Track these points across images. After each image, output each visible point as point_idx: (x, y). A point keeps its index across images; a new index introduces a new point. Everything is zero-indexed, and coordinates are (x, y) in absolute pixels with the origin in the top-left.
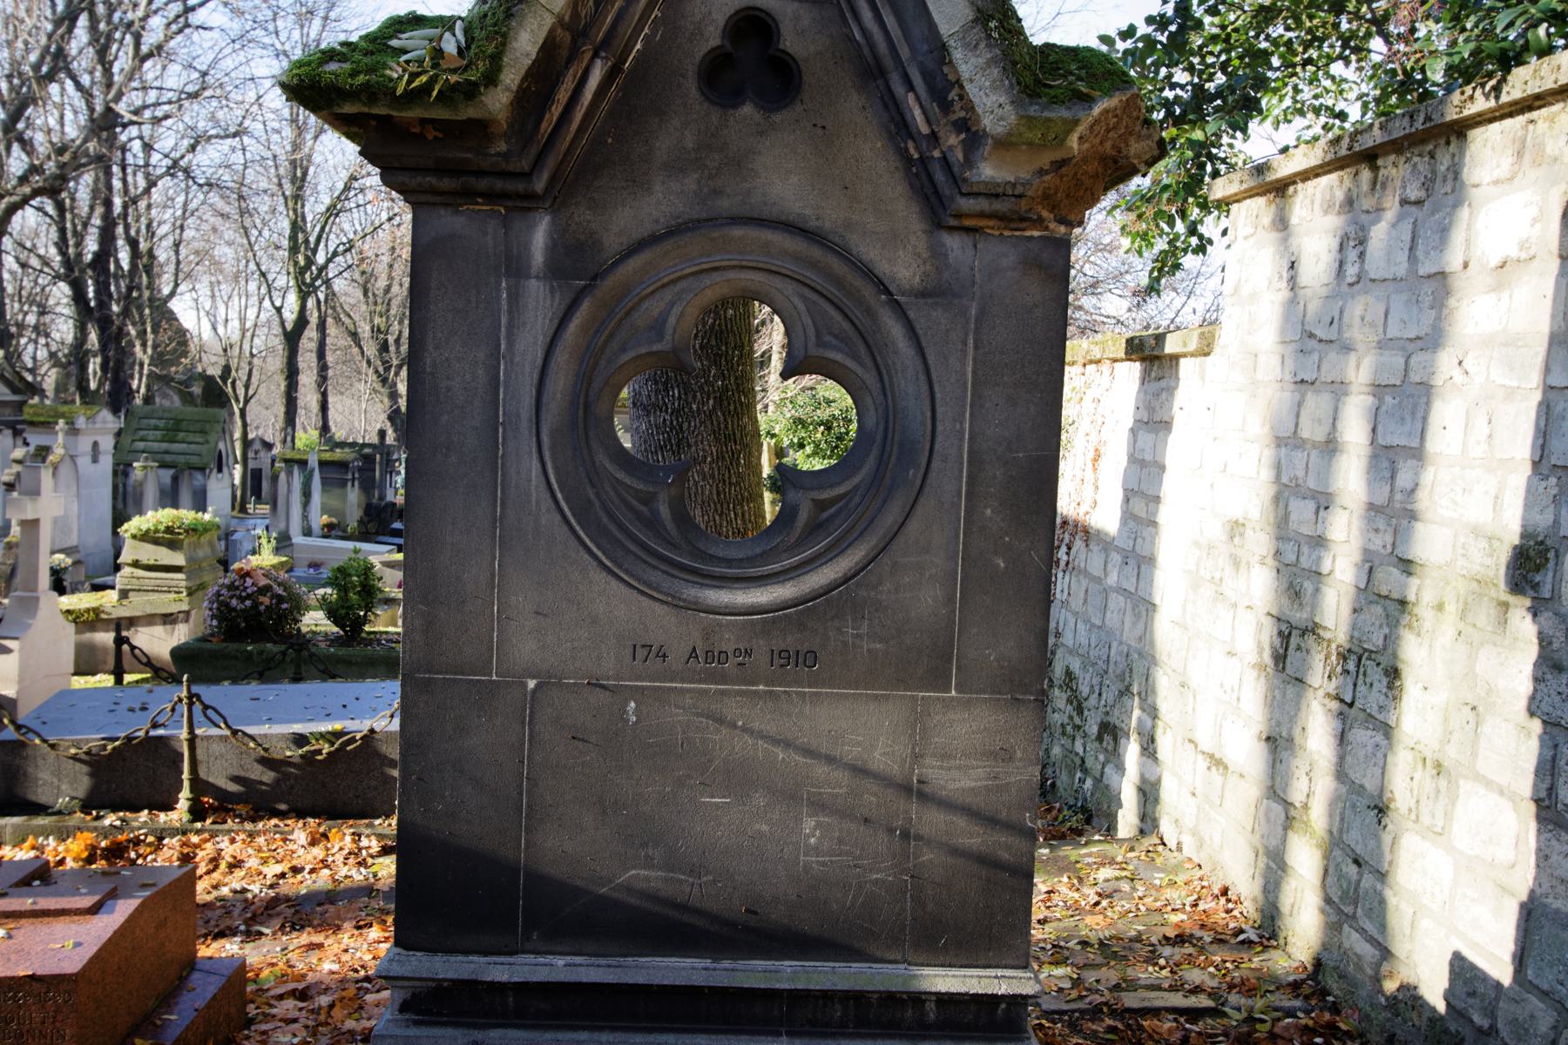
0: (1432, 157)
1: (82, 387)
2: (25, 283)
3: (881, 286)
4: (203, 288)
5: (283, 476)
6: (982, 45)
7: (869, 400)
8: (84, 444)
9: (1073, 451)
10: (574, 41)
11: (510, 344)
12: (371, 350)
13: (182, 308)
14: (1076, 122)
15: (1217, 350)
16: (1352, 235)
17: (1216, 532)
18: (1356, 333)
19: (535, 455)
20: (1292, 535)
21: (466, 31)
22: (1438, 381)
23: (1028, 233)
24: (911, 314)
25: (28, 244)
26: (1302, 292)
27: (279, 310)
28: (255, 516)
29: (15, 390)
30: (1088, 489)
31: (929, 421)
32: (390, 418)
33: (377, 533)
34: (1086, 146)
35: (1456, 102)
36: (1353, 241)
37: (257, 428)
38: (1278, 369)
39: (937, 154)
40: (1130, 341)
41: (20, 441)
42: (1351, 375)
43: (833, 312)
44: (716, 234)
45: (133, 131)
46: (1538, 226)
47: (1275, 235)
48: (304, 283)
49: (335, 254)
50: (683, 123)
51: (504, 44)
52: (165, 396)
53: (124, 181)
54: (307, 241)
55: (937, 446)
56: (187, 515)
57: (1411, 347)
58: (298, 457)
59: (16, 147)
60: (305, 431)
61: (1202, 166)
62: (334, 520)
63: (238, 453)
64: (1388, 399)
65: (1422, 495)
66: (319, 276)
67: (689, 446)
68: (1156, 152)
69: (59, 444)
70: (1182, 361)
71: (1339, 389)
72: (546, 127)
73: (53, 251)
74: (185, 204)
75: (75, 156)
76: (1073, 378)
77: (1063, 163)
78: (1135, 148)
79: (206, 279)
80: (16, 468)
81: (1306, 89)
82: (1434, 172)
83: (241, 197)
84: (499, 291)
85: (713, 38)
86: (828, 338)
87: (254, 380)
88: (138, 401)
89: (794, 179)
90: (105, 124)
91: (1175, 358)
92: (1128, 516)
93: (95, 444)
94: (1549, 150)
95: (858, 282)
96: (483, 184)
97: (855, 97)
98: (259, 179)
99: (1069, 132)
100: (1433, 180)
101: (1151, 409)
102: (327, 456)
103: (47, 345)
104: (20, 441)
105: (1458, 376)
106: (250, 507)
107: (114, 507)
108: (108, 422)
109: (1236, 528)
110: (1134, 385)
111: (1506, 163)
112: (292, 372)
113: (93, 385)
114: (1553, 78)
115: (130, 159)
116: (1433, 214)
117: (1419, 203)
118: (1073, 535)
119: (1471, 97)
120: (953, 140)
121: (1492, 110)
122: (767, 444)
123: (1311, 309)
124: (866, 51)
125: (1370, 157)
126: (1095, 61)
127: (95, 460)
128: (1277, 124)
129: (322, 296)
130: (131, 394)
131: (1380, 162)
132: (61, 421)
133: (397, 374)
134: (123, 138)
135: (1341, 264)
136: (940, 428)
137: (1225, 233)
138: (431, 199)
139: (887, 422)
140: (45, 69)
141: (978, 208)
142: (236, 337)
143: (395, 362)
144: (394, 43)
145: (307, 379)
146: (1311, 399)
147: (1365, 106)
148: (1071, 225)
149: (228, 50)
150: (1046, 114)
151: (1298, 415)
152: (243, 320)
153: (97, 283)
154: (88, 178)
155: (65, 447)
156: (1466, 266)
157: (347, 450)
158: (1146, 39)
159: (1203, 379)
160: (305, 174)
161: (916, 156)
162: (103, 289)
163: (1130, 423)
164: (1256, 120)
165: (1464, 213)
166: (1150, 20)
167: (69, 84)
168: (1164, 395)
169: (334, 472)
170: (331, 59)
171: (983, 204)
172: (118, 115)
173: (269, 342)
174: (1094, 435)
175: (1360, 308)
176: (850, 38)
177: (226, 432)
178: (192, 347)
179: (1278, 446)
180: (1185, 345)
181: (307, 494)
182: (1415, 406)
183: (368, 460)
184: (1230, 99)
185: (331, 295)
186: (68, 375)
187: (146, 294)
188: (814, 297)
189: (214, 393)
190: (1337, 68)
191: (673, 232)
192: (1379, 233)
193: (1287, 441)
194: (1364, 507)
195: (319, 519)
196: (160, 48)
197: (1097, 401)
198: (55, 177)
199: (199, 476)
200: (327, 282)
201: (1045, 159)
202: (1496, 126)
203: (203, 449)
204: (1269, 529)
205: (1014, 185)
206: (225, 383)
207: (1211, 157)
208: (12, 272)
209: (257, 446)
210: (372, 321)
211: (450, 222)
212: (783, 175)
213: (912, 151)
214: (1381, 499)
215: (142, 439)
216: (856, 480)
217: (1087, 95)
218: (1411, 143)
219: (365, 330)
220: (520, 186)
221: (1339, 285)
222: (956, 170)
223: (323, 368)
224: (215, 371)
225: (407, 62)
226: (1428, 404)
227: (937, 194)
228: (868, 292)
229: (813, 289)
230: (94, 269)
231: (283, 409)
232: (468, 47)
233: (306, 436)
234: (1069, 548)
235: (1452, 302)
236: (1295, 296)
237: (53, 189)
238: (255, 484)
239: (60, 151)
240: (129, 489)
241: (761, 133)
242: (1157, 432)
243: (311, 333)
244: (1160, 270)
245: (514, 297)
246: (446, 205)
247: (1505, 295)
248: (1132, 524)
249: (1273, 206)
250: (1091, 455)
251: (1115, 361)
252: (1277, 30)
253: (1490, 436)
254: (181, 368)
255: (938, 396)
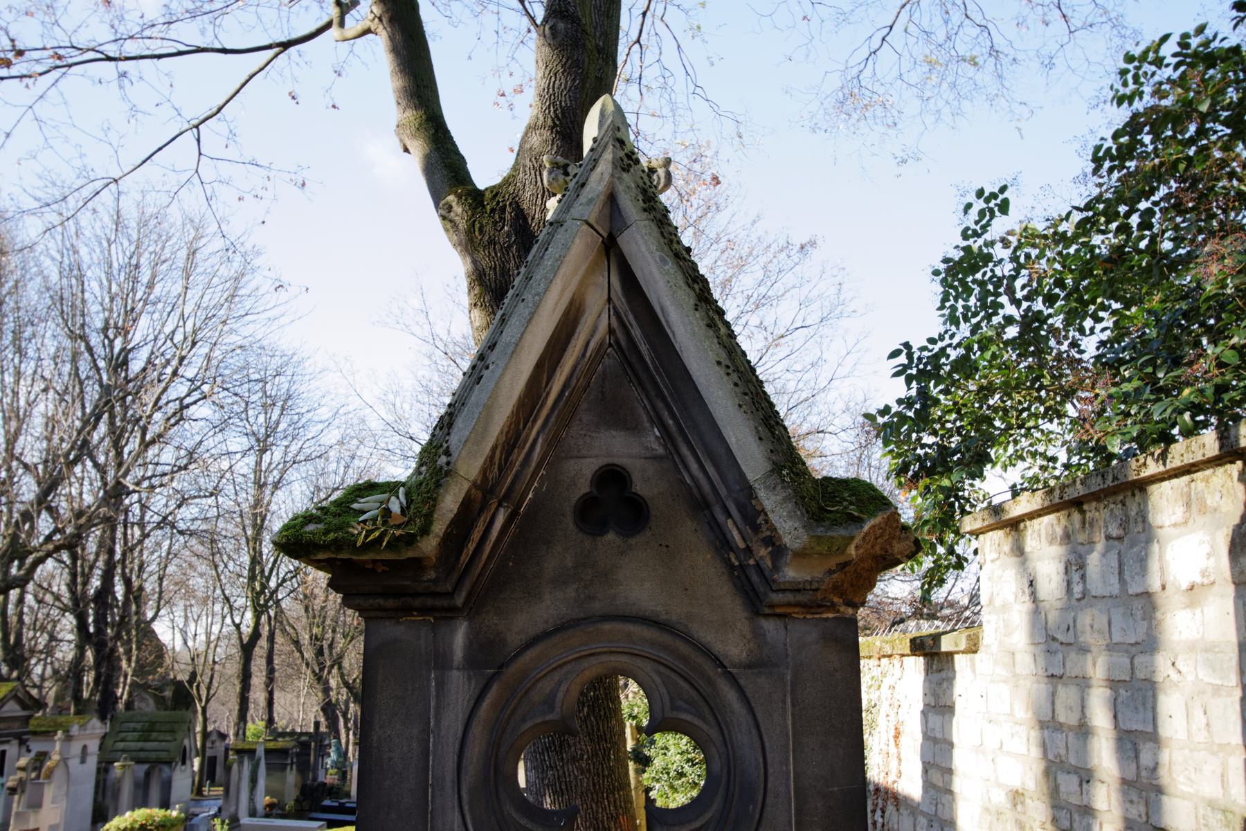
0: (1124, 505)
1: (77, 697)
2: (40, 615)
3: (717, 661)
4: (179, 612)
5: (235, 767)
6: (779, 487)
7: (713, 750)
8: (76, 748)
9: (878, 729)
10: (484, 497)
11: (438, 721)
12: (309, 654)
13: (162, 629)
14: (852, 538)
15: (982, 649)
16: (1073, 562)
17: (1000, 798)
18: (1088, 638)
19: (457, 809)
20: (1064, 804)
21: (407, 494)
22: (1159, 678)
23: (825, 616)
24: (742, 682)
25: (45, 585)
26: (1042, 604)
27: (238, 626)
28: (209, 798)
29: (24, 707)
30: (892, 761)
31: (762, 765)
32: (323, 709)
33: (311, 810)
34: (861, 551)
35: (1134, 467)
36: (1075, 566)
37: (215, 722)
38: (1032, 666)
39: (752, 562)
40: (913, 641)
41: (24, 749)
42: (1090, 671)
43: (682, 683)
44: (591, 629)
45: (135, 497)
46: (1212, 560)
47: (1014, 560)
48: (259, 605)
49: (284, 580)
50: (565, 548)
51: (434, 506)
52: (143, 699)
53: (125, 534)
54: (262, 571)
55: (769, 785)
56: (158, 813)
57: (1133, 650)
58: (247, 747)
59: (44, 515)
60: (254, 722)
61: (952, 505)
62: (275, 800)
63: (199, 744)
64: (1122, 691)
65: (1163, 772)
66: (271, 597)
67: (569, 746)
68: (914, 549)
69: (56, 749)
70: (956, 657)
71: (1083, 683)
72: (464, 558)
73: (64, 588)
74: (170, 548)
75: (89, 519)
76: (869, 670)
77: (846, 564)
78: (897, 547)
79: (181, 604)
80: (21, 774)
81: (1023, 439)
82: (1127, 516)
83: (213, 541)
84: (429, 681)
85: (584, 488)
86: (680, 703)
87: (215, 684)
88: (121, 706)
89: (647, 585)
90: (115, 494)
91: (950, 655)
92: (928, 785)
93: (85, 747)
94: (1209, 502)
95: (700, 660)
96: (417, 602)
97: (689, 523)
98: (227, 527)
99: (849, 544)
100: (1127, 522)
101: (935, 695)
102: (271, 745)
103: (52, 663)
104: (24, 749)
105: (1174, 676)
106: (206, 789)
107: (95, 801)
108: (97, 727)
109: (1017, 797)
110: (920, 676)
111: (1178, 513)
112: (246, 676)
113: (86, 694)
114: (1201, 452)
115: (131, 519)
116: (1132, 547)
117: (1119, 538)
118: (885, 800)
119: (1145, 464)
120: (763, 552)
121: (1162, 473)
122: (629, 725)
123: (1050, 617)
124: (695, 491)
125: (1077, 504)
126: (861, 489)
127: (83, 761)
128: (1005, 468)
129: (272, 613)
130: (117, 700)
131: (1085, 507)
132: (60, 733)
133: (329, 673)
134: (127, 502)
135: (1069, 583)
136: (770, 771)
137: (976, 552)
138: (379, 614)
139: (729, 768)
140: (71, 457)
141: (786, 600)
142: (202, 648)
143: (328, 663)
144: (355, 506)
145: (258, 680)
146: (1061, 690)
147: (1069, 451)
148: (856, 607)
149: (211, 433)
150: (830, 533)
151: (1053, 703)
152: (208, 634)
153: (96, 614)
154: (97, 532)
155: (60, 754)
156: (1164, 588)
157: (287, 739)
158: (898, 414)
159: (974, 671)
160: (263, 521)
161: (737, 564)
162: (100, 620)
163: (921, 706)
164: (989, 466)
165: (1155, 547)
166: (900, 402)
167: (89, 463)
168: (945, 684)
169: (277, 758)
170: (310, 522)
171: (789, 597)
172: (125, 487)
173: (227, 651)
174: (893, 717)
175: (1086, 619)
176: (683, 482)
177: (190, 729)
178: (168, 661)
179: (1042, 728)
180: (956, 645)
181: (254, 781)
182: (1144, 697)
183: (305, 746)
184: (967, 455)
185: (280, 611)
186: (66, 688)
187: (135, 618)
188: (667, 672)
189: (182, 697)
190: (1046, 426)
191: (559, 629)
192: (1094, 560)
193: (1048, 725)
194: (1118, 781)
195: (263, 800)
196: (160, 436)
197: (890, 688)
198: (72, 536)
199: (166, 769)
200: (278, 602)
201: (832, 563)
202: (1166, 484)
203: (171, 746)
204: (1044, 798)
205: (811, 583)
206: (191, 687)
207: (957, 498)
208: (30, 608)
209: (214, 737)
210: (311, 631)
211: (392, 630)
212: (639, 582)
213: (733, 560)
214: (1131, 774)
215: (122, 741)
216: (707, 816)
217: (858, 518)
218: (1103, 499)
219: (305, 638)
220: (446, 603)
221: (1069, 599)
222: (766, 573)
223: (271, 671)
224: (183, 677)
225: (364, 522)
226: (1154, 697)
227: (754, 589)
228: (708, 667)
229: (666, 666)
230: (96, 604)
231: (237, 707)
232: (408, 507)
233: (255, 726)
234: (883, 812)
235: (1158, 615)
236: (1037, 607)
237: (73, 545)
238: (209, 771)
239: (79, 514)
240: (109, 783)
241: (622, 553)
242: (943, 714)
243: (263, 642)
244: (930, 583)
245: (441, 685)
246: (390, 618)
247: (1198, 611)
248: (932, 792)
249: (1010, 538)
250: (892, 732)
251: (903, 655)
252: (994, 400)
253: (1208, 725)
254: (157, 676)
255: (767, 745)
